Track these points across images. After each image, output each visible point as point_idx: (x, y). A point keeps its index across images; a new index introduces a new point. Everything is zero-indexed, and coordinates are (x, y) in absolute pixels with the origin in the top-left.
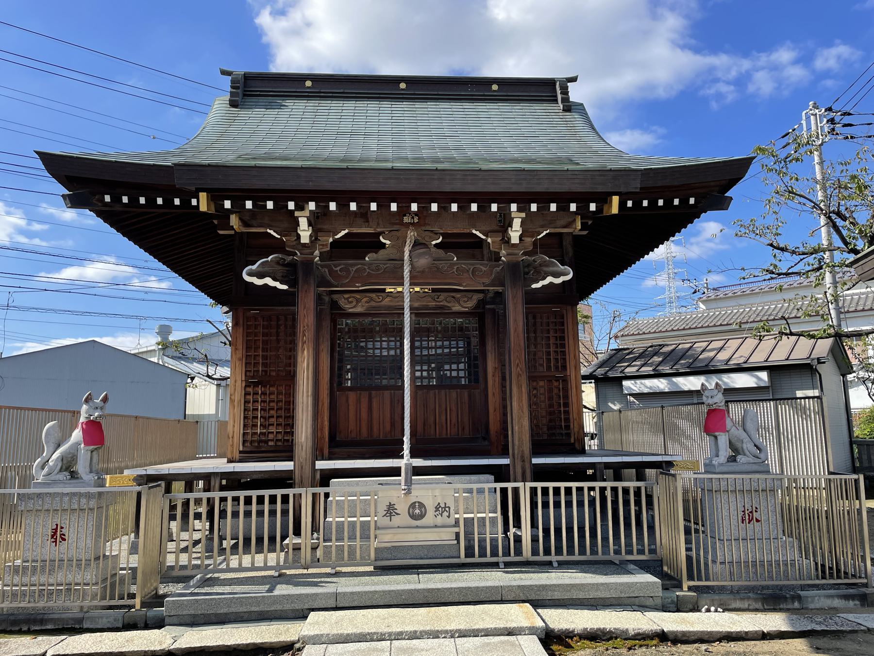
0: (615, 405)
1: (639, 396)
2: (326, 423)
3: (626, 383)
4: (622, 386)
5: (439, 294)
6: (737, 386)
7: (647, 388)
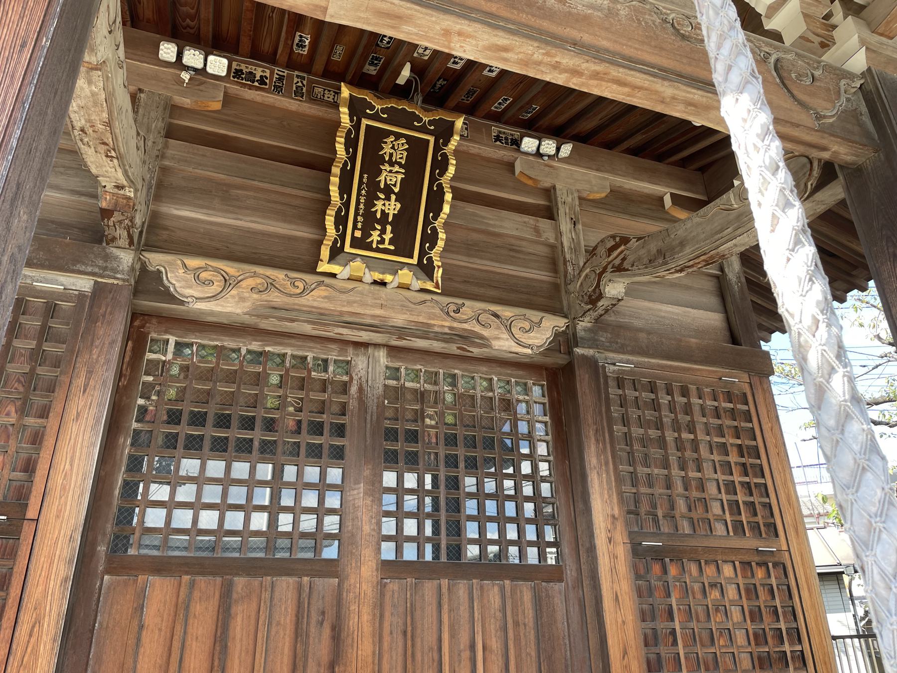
5: (459, 301)
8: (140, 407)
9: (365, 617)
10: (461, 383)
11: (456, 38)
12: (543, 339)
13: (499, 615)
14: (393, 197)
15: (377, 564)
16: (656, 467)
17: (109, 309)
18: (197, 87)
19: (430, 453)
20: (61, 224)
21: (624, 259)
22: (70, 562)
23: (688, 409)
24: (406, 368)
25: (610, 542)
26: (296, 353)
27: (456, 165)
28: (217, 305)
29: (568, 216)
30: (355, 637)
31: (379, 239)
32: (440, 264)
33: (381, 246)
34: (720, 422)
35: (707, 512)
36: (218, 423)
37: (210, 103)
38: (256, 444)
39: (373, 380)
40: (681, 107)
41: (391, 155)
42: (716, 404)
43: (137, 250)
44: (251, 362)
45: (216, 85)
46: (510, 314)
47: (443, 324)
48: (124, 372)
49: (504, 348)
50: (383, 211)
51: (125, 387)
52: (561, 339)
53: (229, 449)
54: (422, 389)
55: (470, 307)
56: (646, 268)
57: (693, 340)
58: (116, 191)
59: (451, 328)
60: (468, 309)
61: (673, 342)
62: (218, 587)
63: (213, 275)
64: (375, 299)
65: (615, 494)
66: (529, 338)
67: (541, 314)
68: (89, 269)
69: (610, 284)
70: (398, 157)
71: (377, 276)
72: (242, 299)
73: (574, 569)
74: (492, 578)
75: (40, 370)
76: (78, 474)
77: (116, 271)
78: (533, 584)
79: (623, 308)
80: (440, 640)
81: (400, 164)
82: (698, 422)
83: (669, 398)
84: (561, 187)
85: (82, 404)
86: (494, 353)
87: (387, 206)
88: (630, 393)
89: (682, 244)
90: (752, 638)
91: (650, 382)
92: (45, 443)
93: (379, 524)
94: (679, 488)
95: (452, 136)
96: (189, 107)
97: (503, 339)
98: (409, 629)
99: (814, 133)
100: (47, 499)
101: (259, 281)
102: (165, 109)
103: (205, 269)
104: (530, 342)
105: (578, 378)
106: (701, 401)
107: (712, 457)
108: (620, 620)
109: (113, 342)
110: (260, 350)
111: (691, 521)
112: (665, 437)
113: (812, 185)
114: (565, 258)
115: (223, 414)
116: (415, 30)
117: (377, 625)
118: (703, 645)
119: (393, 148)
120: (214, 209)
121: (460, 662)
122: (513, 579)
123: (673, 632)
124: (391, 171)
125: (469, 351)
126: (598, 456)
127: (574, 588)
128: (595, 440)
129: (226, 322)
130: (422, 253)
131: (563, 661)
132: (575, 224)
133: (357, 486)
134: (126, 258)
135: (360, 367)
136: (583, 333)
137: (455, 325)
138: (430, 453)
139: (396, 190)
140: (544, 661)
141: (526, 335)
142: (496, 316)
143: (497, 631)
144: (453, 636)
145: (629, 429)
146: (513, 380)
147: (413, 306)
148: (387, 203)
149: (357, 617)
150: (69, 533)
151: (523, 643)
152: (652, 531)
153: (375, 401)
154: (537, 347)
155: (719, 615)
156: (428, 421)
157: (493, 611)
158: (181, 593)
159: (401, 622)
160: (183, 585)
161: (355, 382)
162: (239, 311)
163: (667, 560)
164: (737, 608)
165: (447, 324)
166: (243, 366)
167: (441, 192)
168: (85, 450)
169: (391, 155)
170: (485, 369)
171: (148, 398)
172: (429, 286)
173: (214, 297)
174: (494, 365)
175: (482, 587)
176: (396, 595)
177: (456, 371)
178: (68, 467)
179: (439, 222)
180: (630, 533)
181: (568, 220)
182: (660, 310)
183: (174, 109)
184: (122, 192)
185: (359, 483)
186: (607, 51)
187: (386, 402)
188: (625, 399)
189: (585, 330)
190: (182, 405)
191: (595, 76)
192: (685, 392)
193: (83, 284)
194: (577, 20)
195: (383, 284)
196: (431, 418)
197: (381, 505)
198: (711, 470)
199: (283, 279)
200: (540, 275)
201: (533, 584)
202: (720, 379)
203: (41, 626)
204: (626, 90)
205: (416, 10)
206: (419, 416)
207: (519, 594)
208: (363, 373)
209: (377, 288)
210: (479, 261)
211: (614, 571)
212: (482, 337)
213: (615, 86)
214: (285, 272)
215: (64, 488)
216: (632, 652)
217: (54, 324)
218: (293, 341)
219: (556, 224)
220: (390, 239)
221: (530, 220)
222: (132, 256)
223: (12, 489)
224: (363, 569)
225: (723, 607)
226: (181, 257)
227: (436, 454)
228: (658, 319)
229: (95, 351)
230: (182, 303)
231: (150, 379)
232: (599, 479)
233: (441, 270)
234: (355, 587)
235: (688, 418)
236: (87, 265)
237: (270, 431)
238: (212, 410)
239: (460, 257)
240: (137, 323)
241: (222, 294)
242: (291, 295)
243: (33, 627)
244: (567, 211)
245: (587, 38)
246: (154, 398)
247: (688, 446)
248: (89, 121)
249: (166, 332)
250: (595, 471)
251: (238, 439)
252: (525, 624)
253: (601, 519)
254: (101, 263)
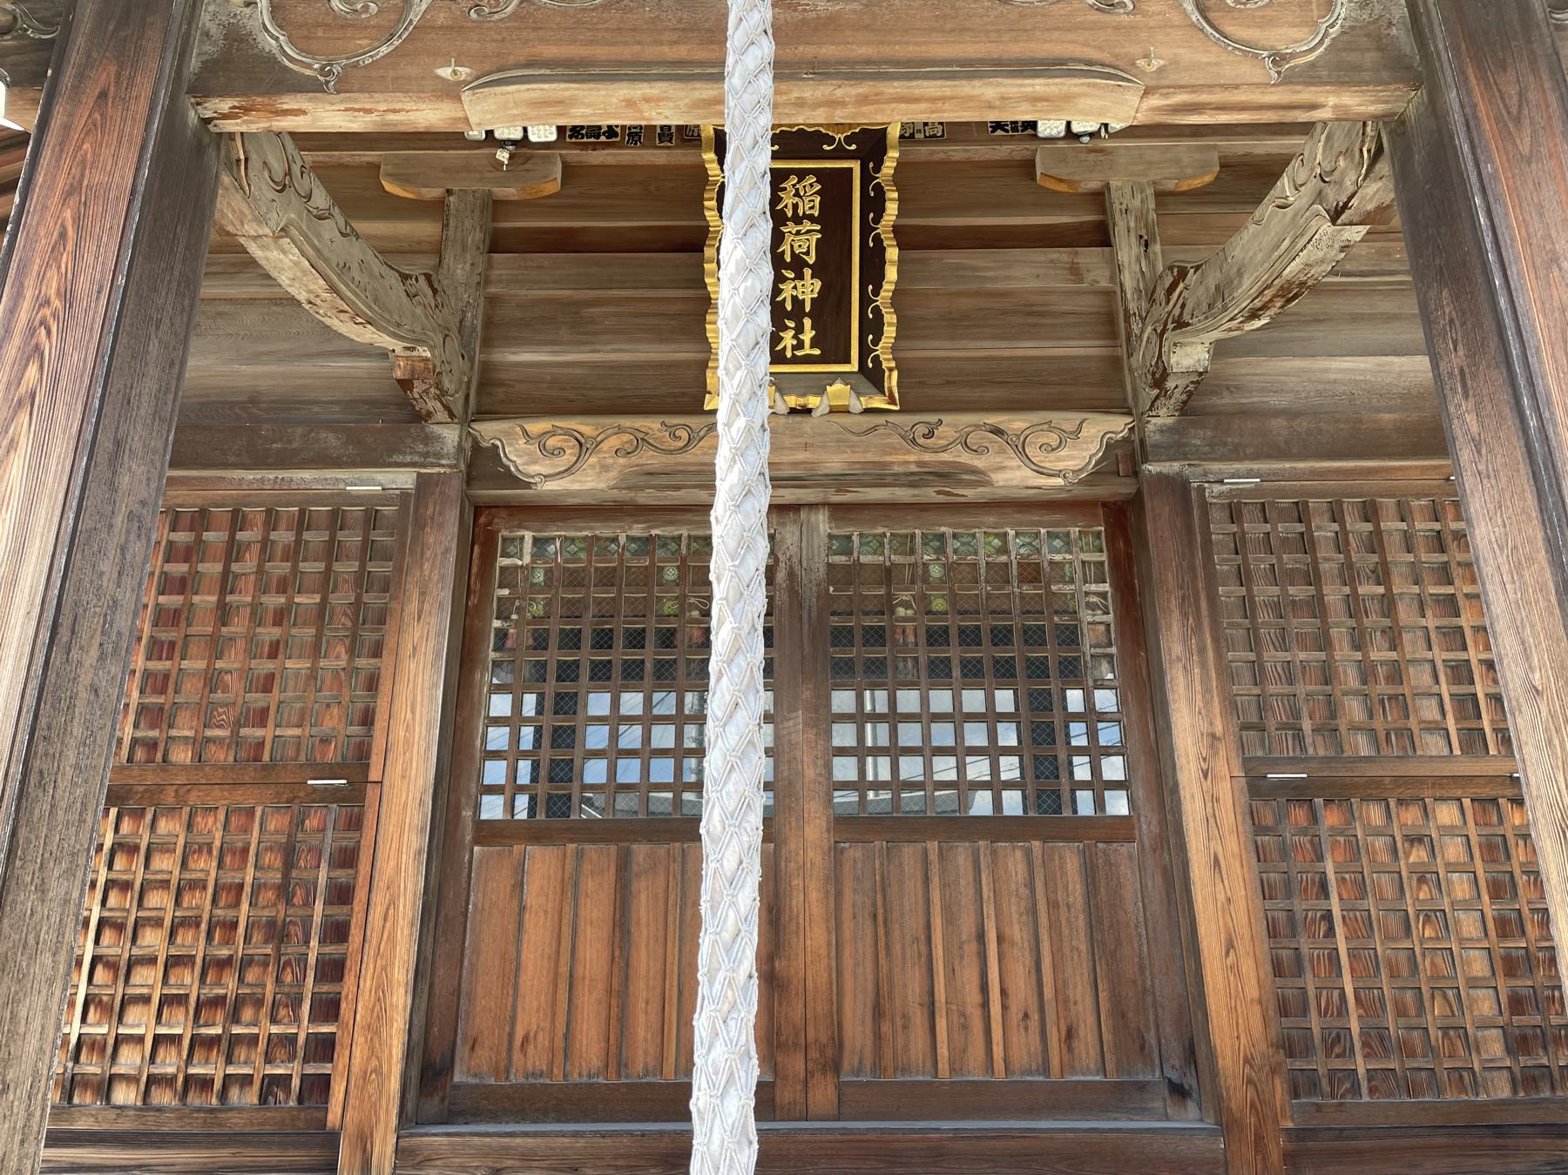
5: (933, 418)
8: (498, 631)
9: (814, 896)
10: (952, 545)
11: (645, 107)
12: (1084, 458)
13: (1024, 892)
14: (808, 272)
15: (828, 822)
16: (1304, 648)
17: (438, 508)
18: (522, 167)
19: (905, 659)
20: (373, 403)
21: (1183, 306)
22: (423, 829)
23: (1375, 542)
24: (861, 535)
25: (1206, 777)
26: (693, 533)
27: (900, 199)
28: (573, 481)
29: (1132, 234)
30: (801, 921)
31: (795, 342)
32: (893, 364)
33: (799, 353)
34: (1444, 558)
35: (1407, 717)
36: (597, 643)
37: (542, 186)
38: (649, 666)
39: (809, 559)
40: (1026, 106)
41: (795, 206)
42: (1437, 526)
43: (461, 424)
44: (635, 554)
45: (547, 156)
46: (1024, 425)
47: (908, 459)
48: (473, 587)
49: (1015, 483)
50: (794, 298)
51: (476, 607)
52: (1119, 452)
53: (613, 676)
54: (888, 564)
55: (951, 424)
56: (1206, 318)
57: (1387, 416)
58: (408, 353)
59: (919, 464)
60: (948, 429)
61: (1342, 426)
62: (613, 858)
63: (564, 441)
64: (796, 437)
65: (1216, 699)
66: (1059, 459)
67: (1077, 417)
68: (408, 459)
69: (1178, 350)
70: (807, 207)
71: (793, 401)
72: (605, 468)
73: (1154, 822)
74: (1011, 838)
75: (366, 598)
76: (421, 724)
77: (438, 455)
78: (1081, 845)
79: (1249, 378)
80: (928, 926)
81: (812, 219)
82: (1396, 563)
83: (1336, 527)
84: (1119, 184)
85: (417, 635)
86: (1002, 493)
87: (800, 289)
88: (1254, 528)
89: (1240, 274)
90: (1491, 925)
91: (1297, 503)
92: (381, 688)
93: (829, 768)
94: (1352, 679)
95: (885, 152)
96: (516, 198)
97: (1011, 468)
98: (880, 912)
99: (1273, 89)
100: (390, 757)
101: (626, 437)
102: (482, 212)
103: (552, 433)
104: (1061, 466)
105: (1149, 516)
106: (1404, 526)
107: (1423, 622)
108: (1221, 897)
109: (447, 550)
110: (646, 535)
111: (1372, 732)
112: (1323, 595)
113: (1369, 151)
114: (1126, 311)
115: (603, 630)
116: (589, 111)
117: (832, 905)
118: (1388, 937)
119: (797, 194)
120: (562, 343)
121: (962, 957)
122: (1045, 839)
123: (1328, 916)
124: (798, 233)
125: (957, 495)
126: (1185, 640)
127: (1155, 851)
128: (1181, 612)
129: (593, 502)
130: (864, 351)
131: (1136, 960)
132: (1146, 245)
133: (792, 715)
134: (450, 435)
135: (789, 542)
136: (1158, 437)
137: (927, 457)
138: (905, 659)
139: (811, 260)
140: (1100, 959)
141: (1052, 456)
142: (998, 432)
143: (1021, 915)
144: (950, 919)
145: (1249, 590)
146: (1043, 531)
147: (856, 438)
148: (799, 283)
149: (802, 895)
150: (418, 796)
151: (1066, 932)
152: (1291, 754)
153: (814, 589)
154: (1073, 472)
155: (1425, 888)
156: (901, 611)
157: (1013, 887)
158: (567, 867)
159: (868, 902)
160: (568, 855)
161: (782, 565)
162: (602, 485)
163: (1319, 801)
164: (1465, 876)
165: (912, 458)
166: (622, 560)
167: (880, 249)
168: (426, 692)
169: (795, 206)
170: (992, 519)
171: (507, 618)
172: (879, 402)
173: (568, 471)
174: (1009, 510)
175: (994, 853)
176: (859, 866)
177: (943, 529)
178: (409, 715)
179: (883, 298)
180: (1246, 762)
181: (1133, 240)
182: (1327, 370)
183: (497, 207)
184: (415, 353)
185: (797, 710)
186: (868, 62)
187: (831, 589)
188: (1243, 538)
189: (1162, 430)
190: (548, 624)
191: (864, 100)
192: (1370, 512)
193: (404, 479)
194: (816, 29)
195: (807, 411)
196: (907, 605)
197: (829, 737)
198: (1421, 643)
199: (659, 430)
200: (1083, 348)
201: (1081, 845)
202: (1448, 480)
203: (396, 909)
204: (923, 106)
205: (575, 89)
206: (886, 606)
207: (1057, 861)
208: (794, 550)
209: (798, 418)
210: (972, 344)
211: (1212, 820)
212: (974, 471)
213: (903, 106)
214: (661, 419)
215: (406, 741)
216: (1243, 946)
217: (378, 536)
218: (689, 516)
219: (1112, 252)
220: (812, 339)
221: (1062, 255)
222: (457, 432)
223: (351, 747)
224: (807, 829)
225: (1434, 876)
226: (519, 422)
227: (916, 659)
228: (1321, 387)
229: (426, 565)
230: (528, 485)
231: (506, 592)
232: (1186, 676)
233: (895, 374)
234: (798, 854)
235: (1375, 558)
236: (404, 453)
237: (668, 647)
238: (587, 626)
239: (937, 344)
240: (482, 520)
241: (578, 465)
242: (671, 452)
243: (388, 909)
244: (1132, 224)
245: (829, 51)
246: (514, 617)
247: (1374, 607)
248: (310, 291)
249: (520, 527)
250: (1180, 665)
251: (625, 661)
252: (1068, 906)
253: (1189, 741)
254: (421, 448)
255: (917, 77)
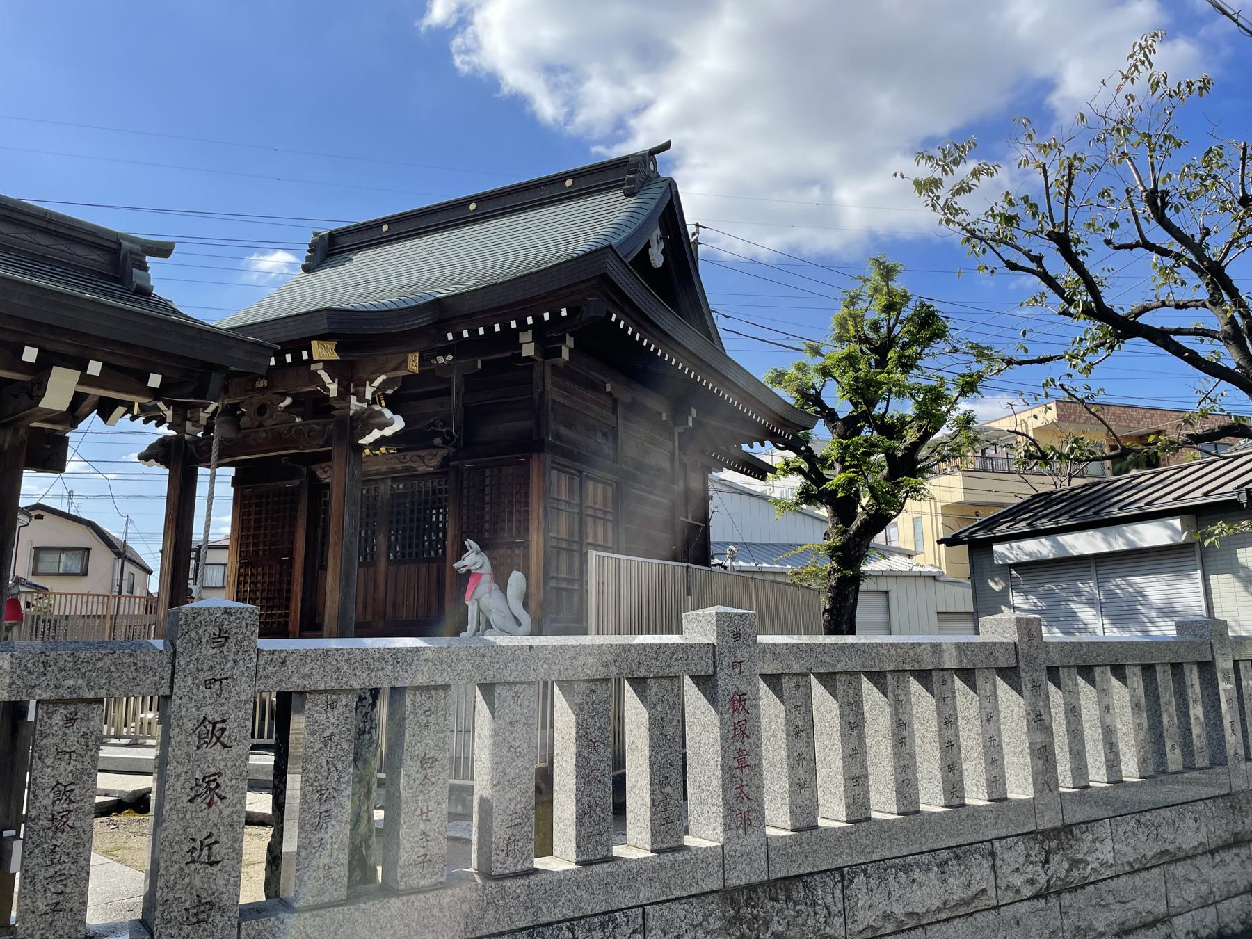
0: (996, 583)
1: (1019, 566)
2: (299, 605)
3: (998, 548)
4: (991, 551)
5: (405, 453)
6: (1145, 545)
7: (1026, 555)
255: (105, 246)
